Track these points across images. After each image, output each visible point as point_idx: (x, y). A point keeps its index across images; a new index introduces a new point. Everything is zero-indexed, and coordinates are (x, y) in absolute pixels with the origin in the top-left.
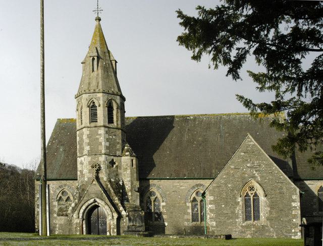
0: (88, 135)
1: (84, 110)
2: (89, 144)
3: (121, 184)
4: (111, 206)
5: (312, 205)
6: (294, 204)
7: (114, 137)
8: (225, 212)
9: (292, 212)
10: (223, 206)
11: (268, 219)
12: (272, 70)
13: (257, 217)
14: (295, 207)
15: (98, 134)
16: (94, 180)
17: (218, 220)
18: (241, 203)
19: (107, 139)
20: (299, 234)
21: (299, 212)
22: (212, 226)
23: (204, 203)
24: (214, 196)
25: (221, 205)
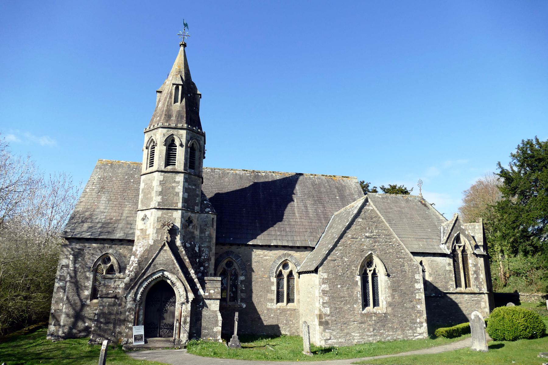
0: (160, 181)
1: (157, 149)
2: (161, 193)
3: (197, 251)
4: (186, 283)
7: (193, 187)
9: (416, 296)
10: (339, 286)
11: (390, 304)
12: (13, 322)
14: (419, 289)
15: (175, 182)
16: (164, 245)
20: (425, 325)
21: (424, 296)
22: (325, 315)
24: (329, 273)
25: (337, 285)
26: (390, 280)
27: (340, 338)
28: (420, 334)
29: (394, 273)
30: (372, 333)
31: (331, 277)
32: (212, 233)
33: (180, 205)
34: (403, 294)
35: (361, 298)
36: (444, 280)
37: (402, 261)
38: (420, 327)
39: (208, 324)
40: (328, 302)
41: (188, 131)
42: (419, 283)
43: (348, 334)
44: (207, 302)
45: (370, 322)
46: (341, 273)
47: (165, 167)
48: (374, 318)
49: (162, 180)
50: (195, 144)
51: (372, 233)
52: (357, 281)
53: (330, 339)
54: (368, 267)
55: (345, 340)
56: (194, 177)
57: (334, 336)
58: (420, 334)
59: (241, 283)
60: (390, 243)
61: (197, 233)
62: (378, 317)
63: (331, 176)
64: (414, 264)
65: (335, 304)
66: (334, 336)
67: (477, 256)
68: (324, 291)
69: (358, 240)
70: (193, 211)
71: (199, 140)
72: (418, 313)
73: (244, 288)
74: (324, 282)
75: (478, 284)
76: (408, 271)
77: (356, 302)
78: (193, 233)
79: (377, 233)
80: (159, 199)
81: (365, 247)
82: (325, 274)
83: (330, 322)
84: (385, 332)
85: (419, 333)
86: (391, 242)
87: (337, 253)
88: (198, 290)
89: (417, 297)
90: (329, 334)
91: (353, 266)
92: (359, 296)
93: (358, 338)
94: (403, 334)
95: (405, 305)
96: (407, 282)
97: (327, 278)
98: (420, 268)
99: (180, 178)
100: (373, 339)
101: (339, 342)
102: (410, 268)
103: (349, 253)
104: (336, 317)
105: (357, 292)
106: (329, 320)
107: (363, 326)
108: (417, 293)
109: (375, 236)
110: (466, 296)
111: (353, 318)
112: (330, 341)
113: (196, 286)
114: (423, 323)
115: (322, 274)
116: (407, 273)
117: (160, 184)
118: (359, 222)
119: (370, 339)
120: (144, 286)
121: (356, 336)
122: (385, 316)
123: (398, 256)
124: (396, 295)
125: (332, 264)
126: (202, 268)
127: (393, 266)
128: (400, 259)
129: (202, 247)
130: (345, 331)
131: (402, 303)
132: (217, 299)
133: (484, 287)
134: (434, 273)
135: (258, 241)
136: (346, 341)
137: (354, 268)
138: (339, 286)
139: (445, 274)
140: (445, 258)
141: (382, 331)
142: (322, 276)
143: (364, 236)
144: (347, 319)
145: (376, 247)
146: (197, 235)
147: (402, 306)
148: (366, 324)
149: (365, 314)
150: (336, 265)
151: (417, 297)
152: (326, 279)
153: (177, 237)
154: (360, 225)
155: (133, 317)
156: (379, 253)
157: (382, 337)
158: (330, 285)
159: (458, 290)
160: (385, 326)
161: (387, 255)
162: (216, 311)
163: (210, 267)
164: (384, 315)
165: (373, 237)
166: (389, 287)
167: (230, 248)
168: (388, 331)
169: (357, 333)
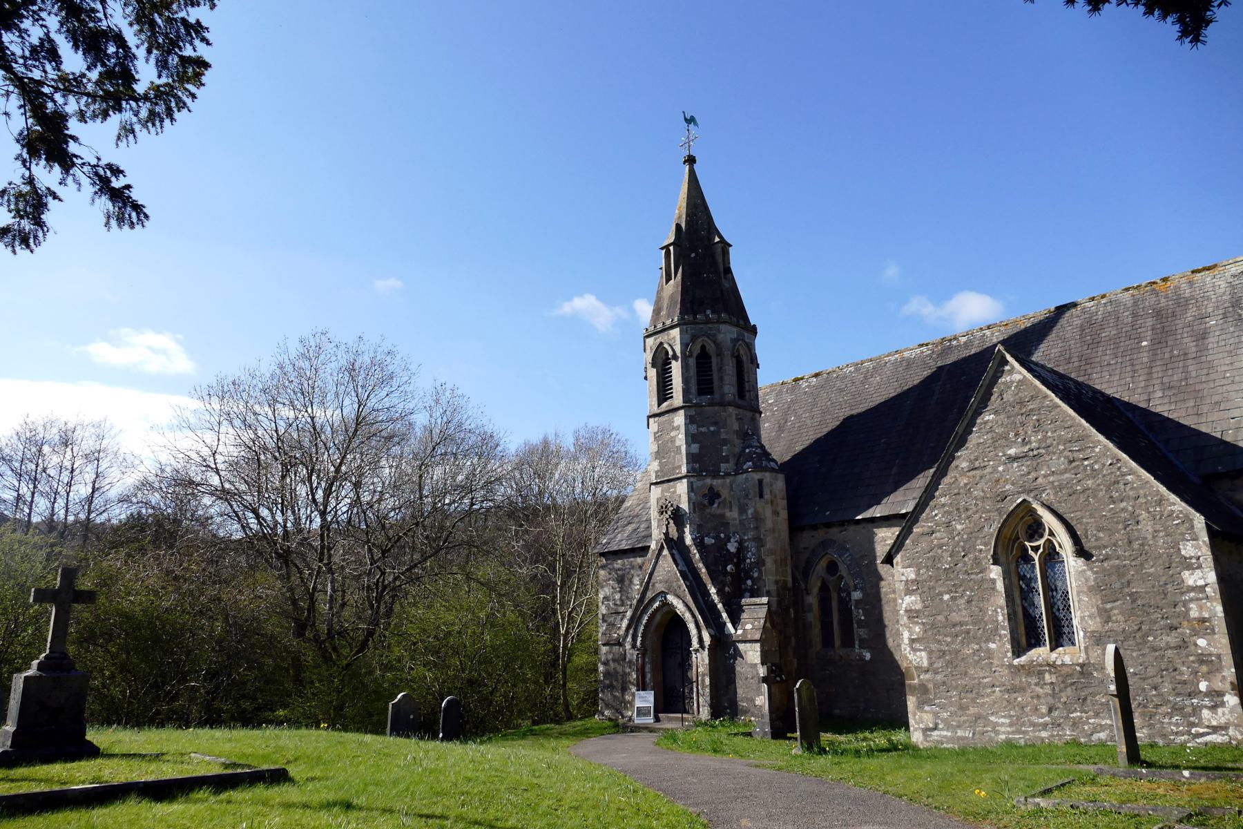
6: (1191, 579)
7: (712, 429)
9: (1188, 610)
10: (946, 597)
13: (1060, 636)
14: (1202, 589)
17: (934, 646)
18: (1000, 586)
19: (693, 436)
23: (1066, 565)
26: (1091, 569)
27: (959, 727)
28: (1215, 729)
29: (1105, 547)
30: (1047, 719)
31: (925, 577)
32: (760, 510)
33: (684, 470)
35: (1006, 624)
37: (1130, 508)
38: (1214, 708)
39: (746, 690)
40: (923, 639)
41: (685, 327)
42: (1200, 567)
43: (978, 717)
44: (741, 646)
45: (1038, 689)
47: (659, 405)
49: (656, 430)
50: (705, 344)
51: (1027, 444)
52: (993, 581)
55: (974, 734)
56: (711, 408)
57: (944, 721)
58: (1215, 729)
59: (856, 607)
60: (1086, 463)
61: (733, 515)
62: (1062, 676)
63: (1154, 283)
64: (1173, 512)
66: (944, 721)
69: (988, 470)
70: (715, 474)
71: (714, 335)
72: (1202, 662)
73: (863, 618)
74: (908, 589)
76: (1154, 537)
77: (993, 634)
78: (723, 516)
79: (1040, 441)
80: (655, 466)
82: (909, 570)
83: (930, 686)
84: (1088, 718)
85: (1208, 727)
86: (1087, 459)
87: (936, 515)
88: (725, 624)
89: (1194, 613)
90: (930, 716)
91: (979, 542)
92: (1000, 618)
93: (1009, 729)
95: (1151, 638)
97: (916, 580)
98: (1195, 522)
99: (679, 419)
100: (1052, 736)
101: (959, 738)
102: (1158, 527)
103: (967, 510)
104: (944, 673)
105: (996, 610)
106: (928, 681)
107: (1019, 699)
108: (1191, 600)
109: (1035, 453)
111: (988, 677)
112: (936, 733)
113: (721, 616)
114: (1223, 695)
115: (902, 570)
116: (1151, 542)
117: (655, 438)
118: (986, 423)
119: (1044, 734)
120: (644, 622)
121: (1003, 724)
122: (1081, 673)
123: (1115, 495)
126: (749, 582)
129: (746, 541)
130: (972, 710)
132: (756, 641)
135: (877, 512)
136: (977, 736)
142: (903, 575)
145: (1040, 480)
146: (735, 519)
147: (1138, 644)
148: (1028, 694)
149: (1023, 666)
150: (935, 545)
151: (1194, 613)
152: (913, 581)
153: (685, 529)
154: (991, 430)
155: (635, 676)
157: (1078, 731)
160: (1085, 700)
161: (1078, 499)
162: (756, 665)
163: (764, 578)
164: (1078, 668)
165: (1031, 454)
166: (1091, 589)
167: (827, 533)
168: (1097, 715)
169: (1003, 717)
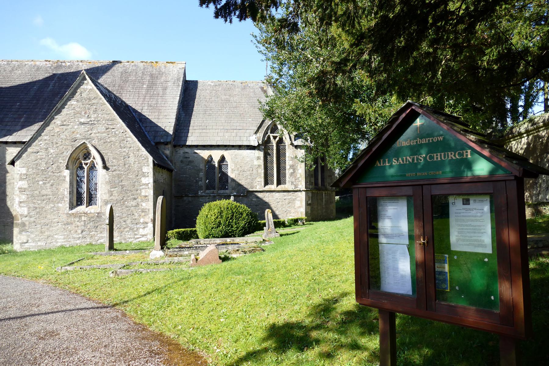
5: (197, 182)
8: (44, 192)
10: (41, 183)
17: (31, 205)
26: (108, 174)
27: (39, 241)
28: (143, 236)
29: (115, 166)
31: (31, 173)
34: (124, 190)
36: (249, 177)
42: (148, 176)
45: (78, 223)
46: (44, 167)
48: (83, 218)
52: (65, 177)
53: (27, 242)
54: (85, 159)
55: (46, 244)
57: (32, 239)
60: (113, 130)
63: (153, 62)
65: (34, 203)
66: (32, 239)
67: (296, 147)
68: (21, 188)
72: (143, 212)
74: (21, 178)
75: (293, 180)
76: (134, 164)
79: (95, 118)
81: (78, 136)
82: (23, 169)
83: (27, 223)
84: (97, 234)
87: (41, 144)
89: (143, 194)
92: (66, 193)
93: (63, 240)
94: (121, 236)
95: (126, 203)
96: (131, 176)
102: (136, 160)
103: (57, 143)
104: (35, 217)
105: (64, 190)
106: (26, 221)
107: (69, 228)
109: (92, 122)
110: (277, 194)
112: (27, 244)
115: (19, 169)
118: (72, 105)
122: (97, 216)
123: (122, 145)
124: (115, 192)
125: (33, 157)
127: (114, 158)
128: (125, 149)
130: (46, 233)
131: (122, 201)
133: (301, 184)
134: (238, 169)
136: (47, 245)
137: (62, 161)
138: (41, 183)
139: (251, 170)
140: (253, 151)
141: (94, 233)
143: (78, 122)
144: (50, 219)
145: (92, 135)
148: (74, 225)
154: (74, 109)
156: (97, 143)
158: (30, 181)
159: (268, 188)
160: (97, 227)
164: (97, 214)
165: (90, 122)
166: (107, 183)
